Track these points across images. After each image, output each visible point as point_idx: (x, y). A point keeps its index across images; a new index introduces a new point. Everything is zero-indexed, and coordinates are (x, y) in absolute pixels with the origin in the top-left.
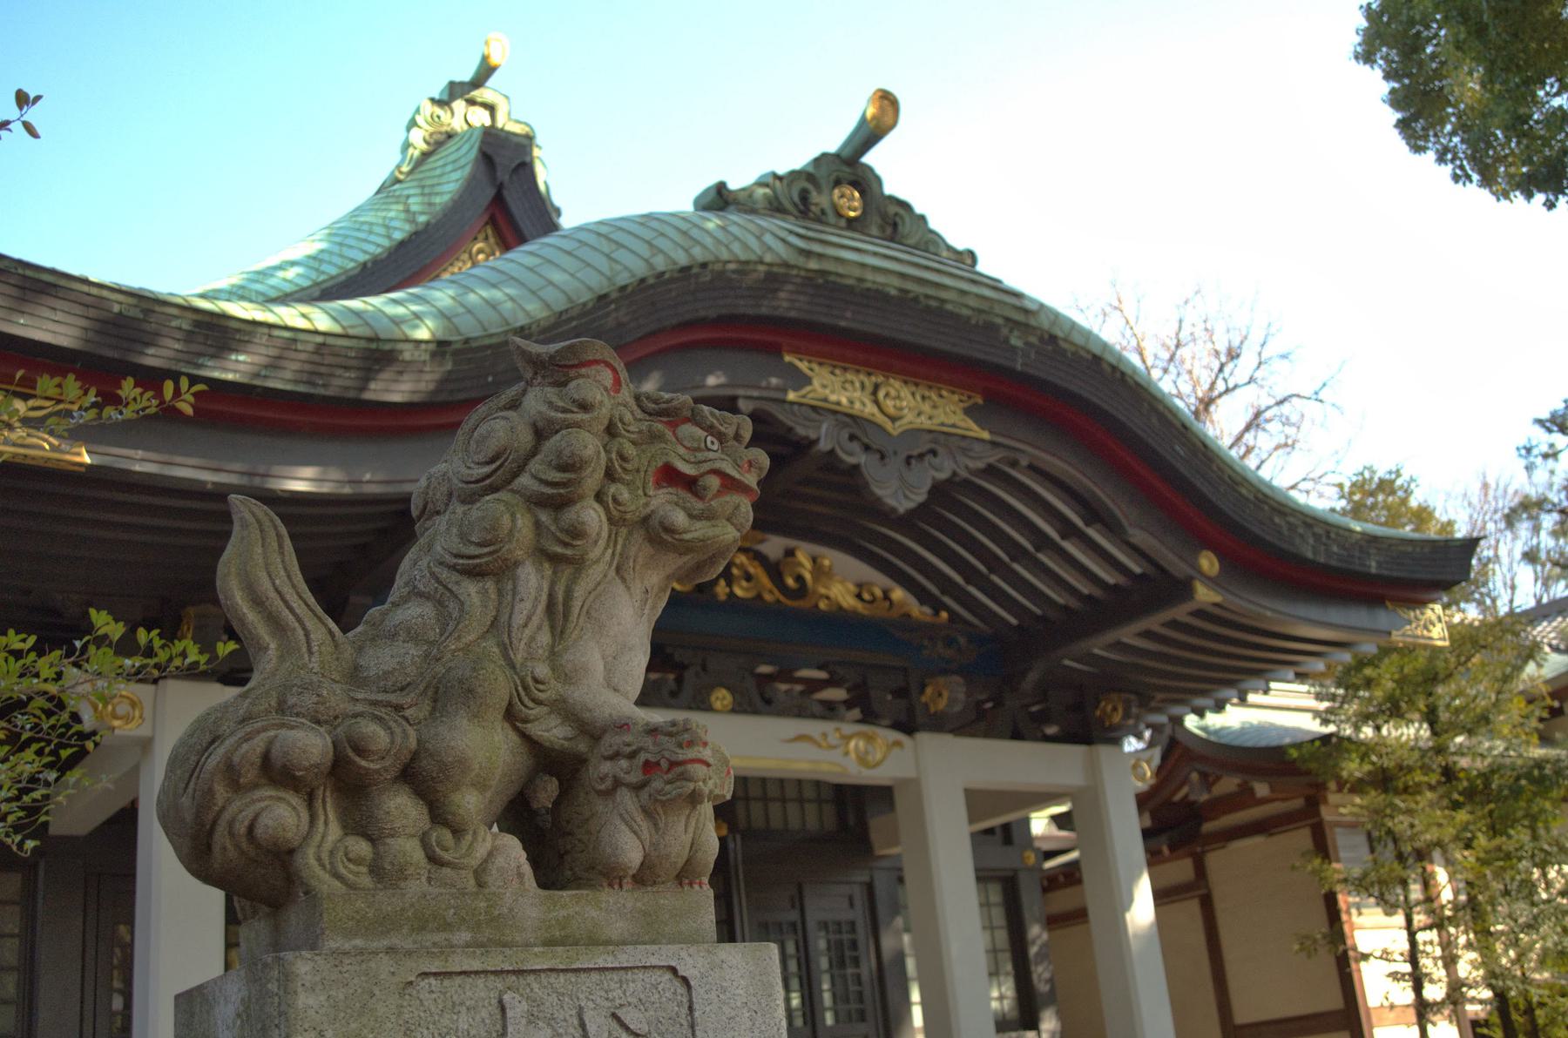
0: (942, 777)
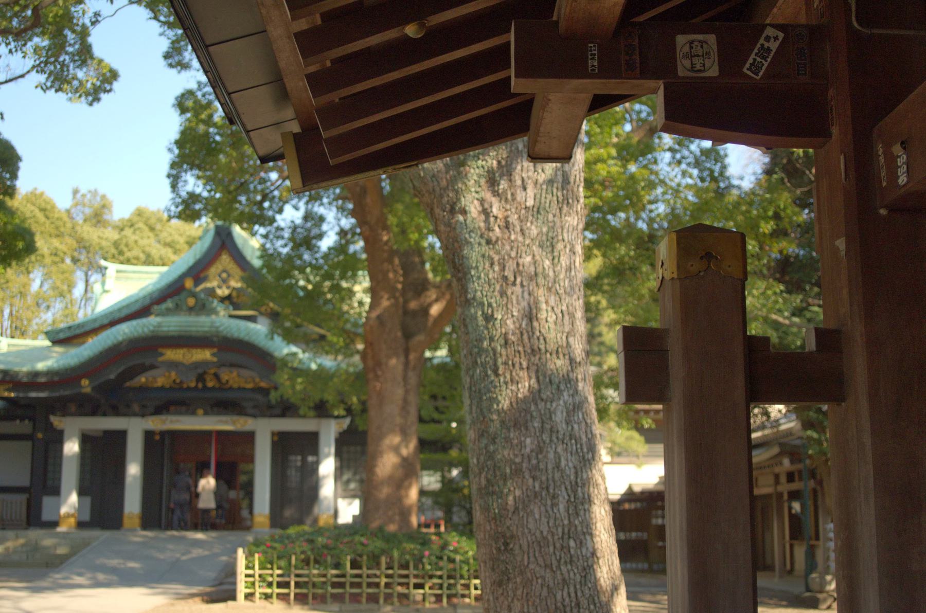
0: (264, 430)
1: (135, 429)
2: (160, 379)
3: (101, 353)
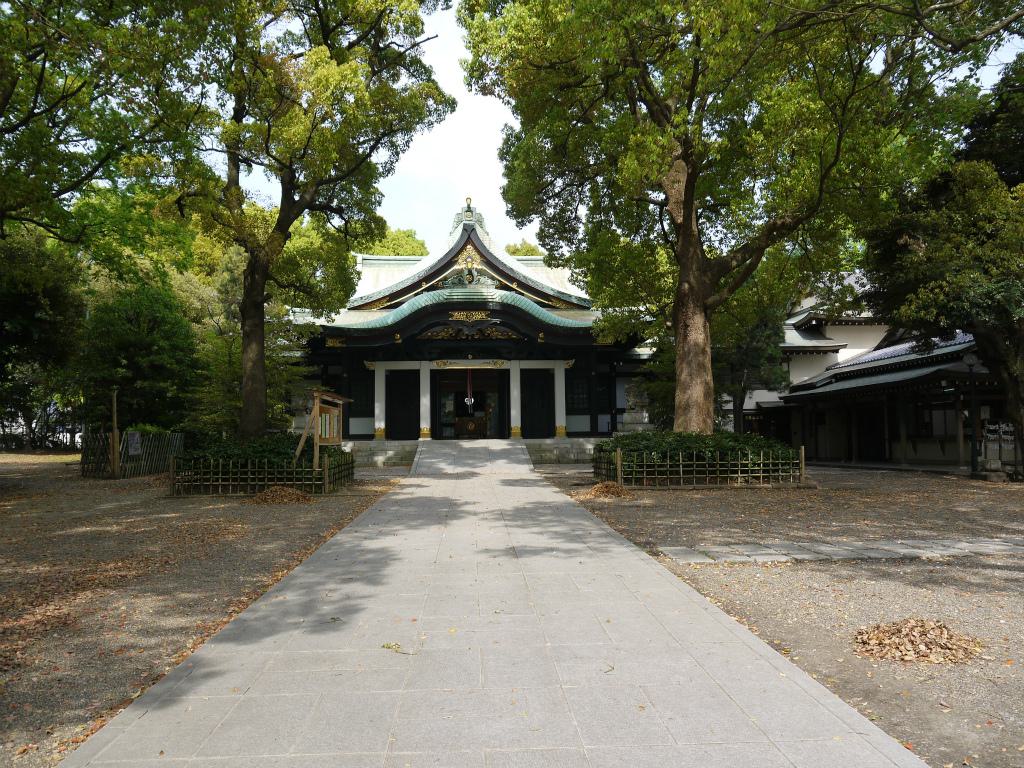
0: (515, 368)
1: (425, 369)
2: (442, 333)
3: (410, 315)
